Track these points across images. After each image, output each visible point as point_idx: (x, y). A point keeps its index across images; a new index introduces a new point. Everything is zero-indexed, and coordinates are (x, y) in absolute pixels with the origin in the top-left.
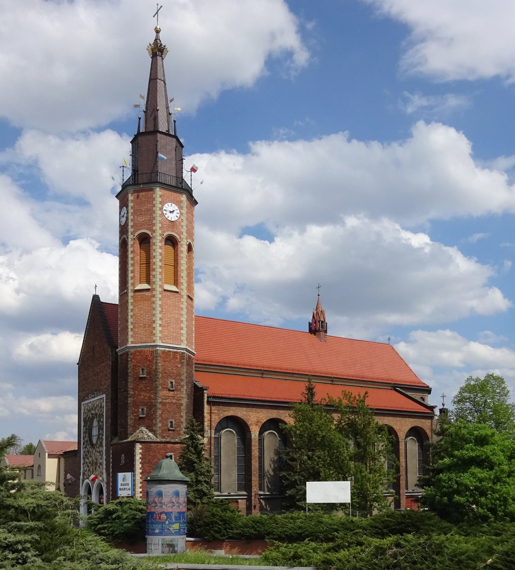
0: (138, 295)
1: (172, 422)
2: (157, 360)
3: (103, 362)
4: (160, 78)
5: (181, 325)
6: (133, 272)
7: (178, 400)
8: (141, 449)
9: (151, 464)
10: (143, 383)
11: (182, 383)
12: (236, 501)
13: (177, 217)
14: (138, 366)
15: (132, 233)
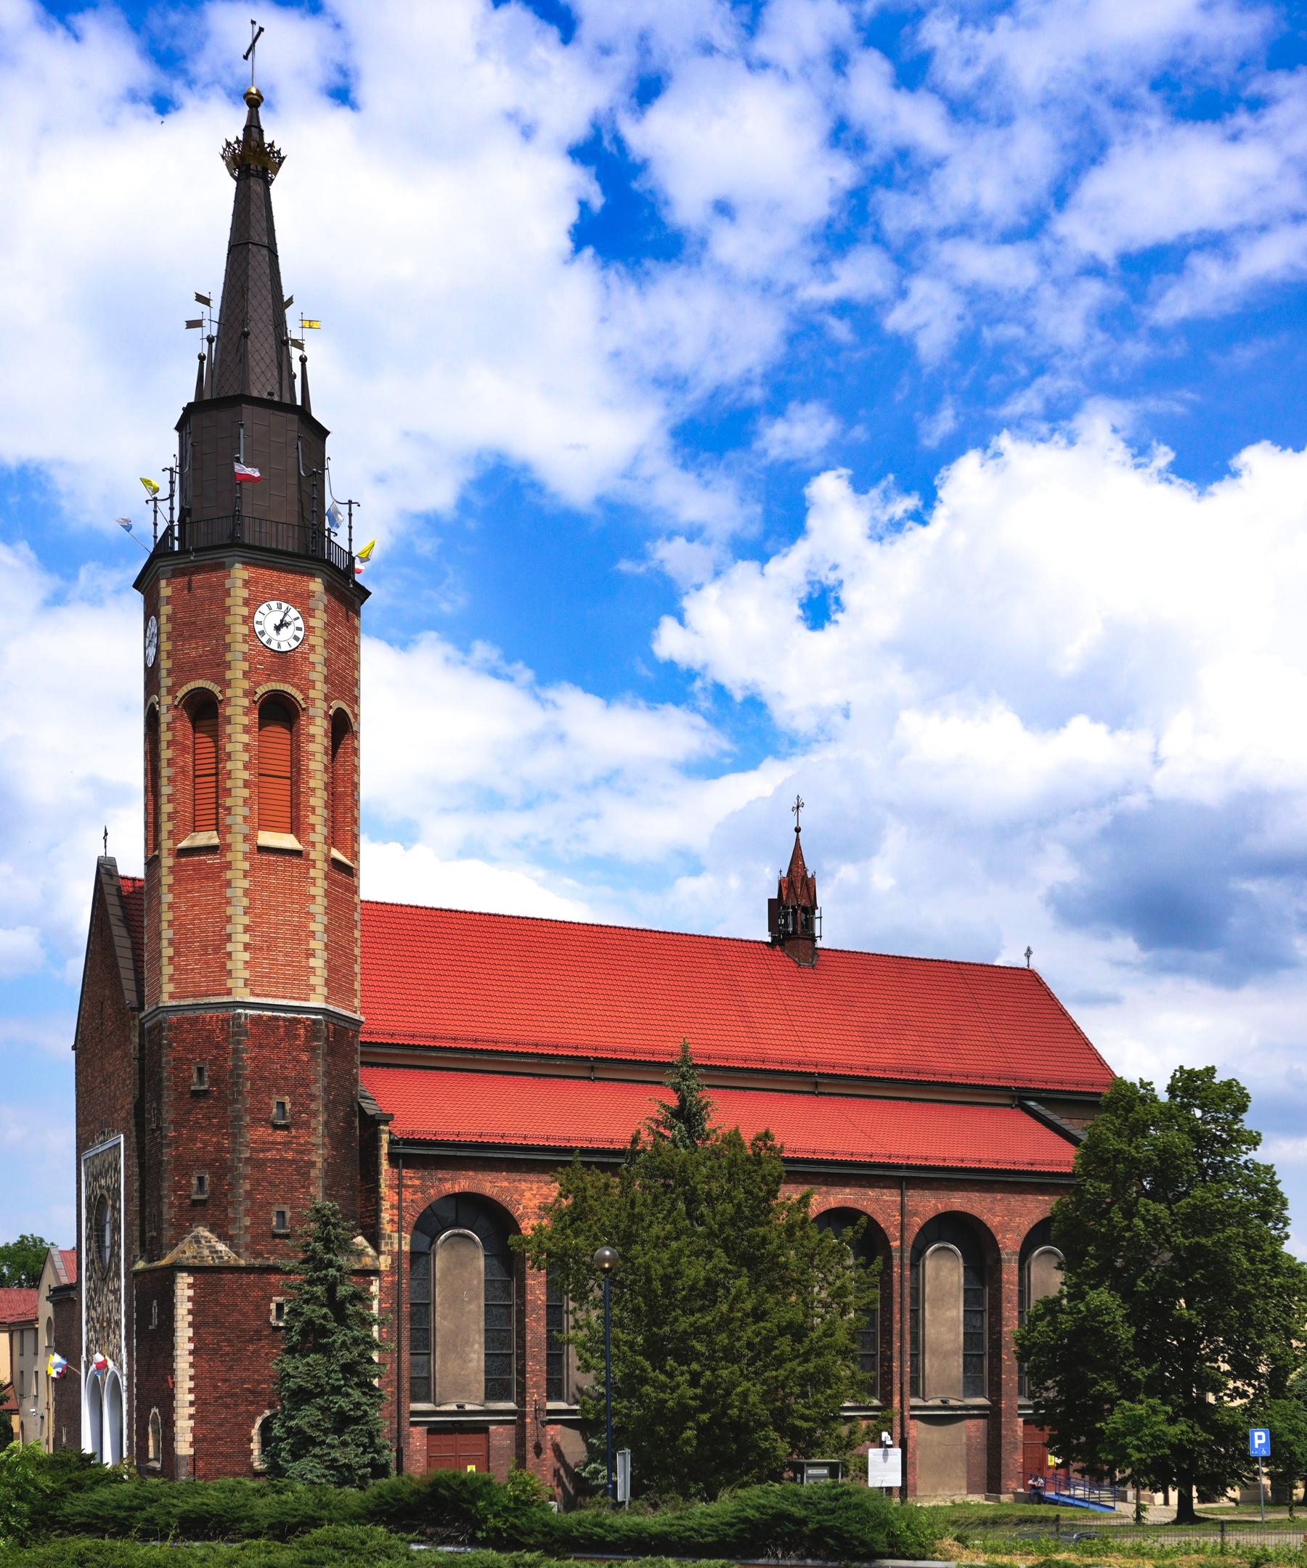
2: (239, 1042)
4: (256, 239)
7: (302, 1152)
8: (190, 1286)
10: (201, 1108)
11: (313, 1106)
12: (482, 1429)
13: (296, 638)
15: (171, 691)
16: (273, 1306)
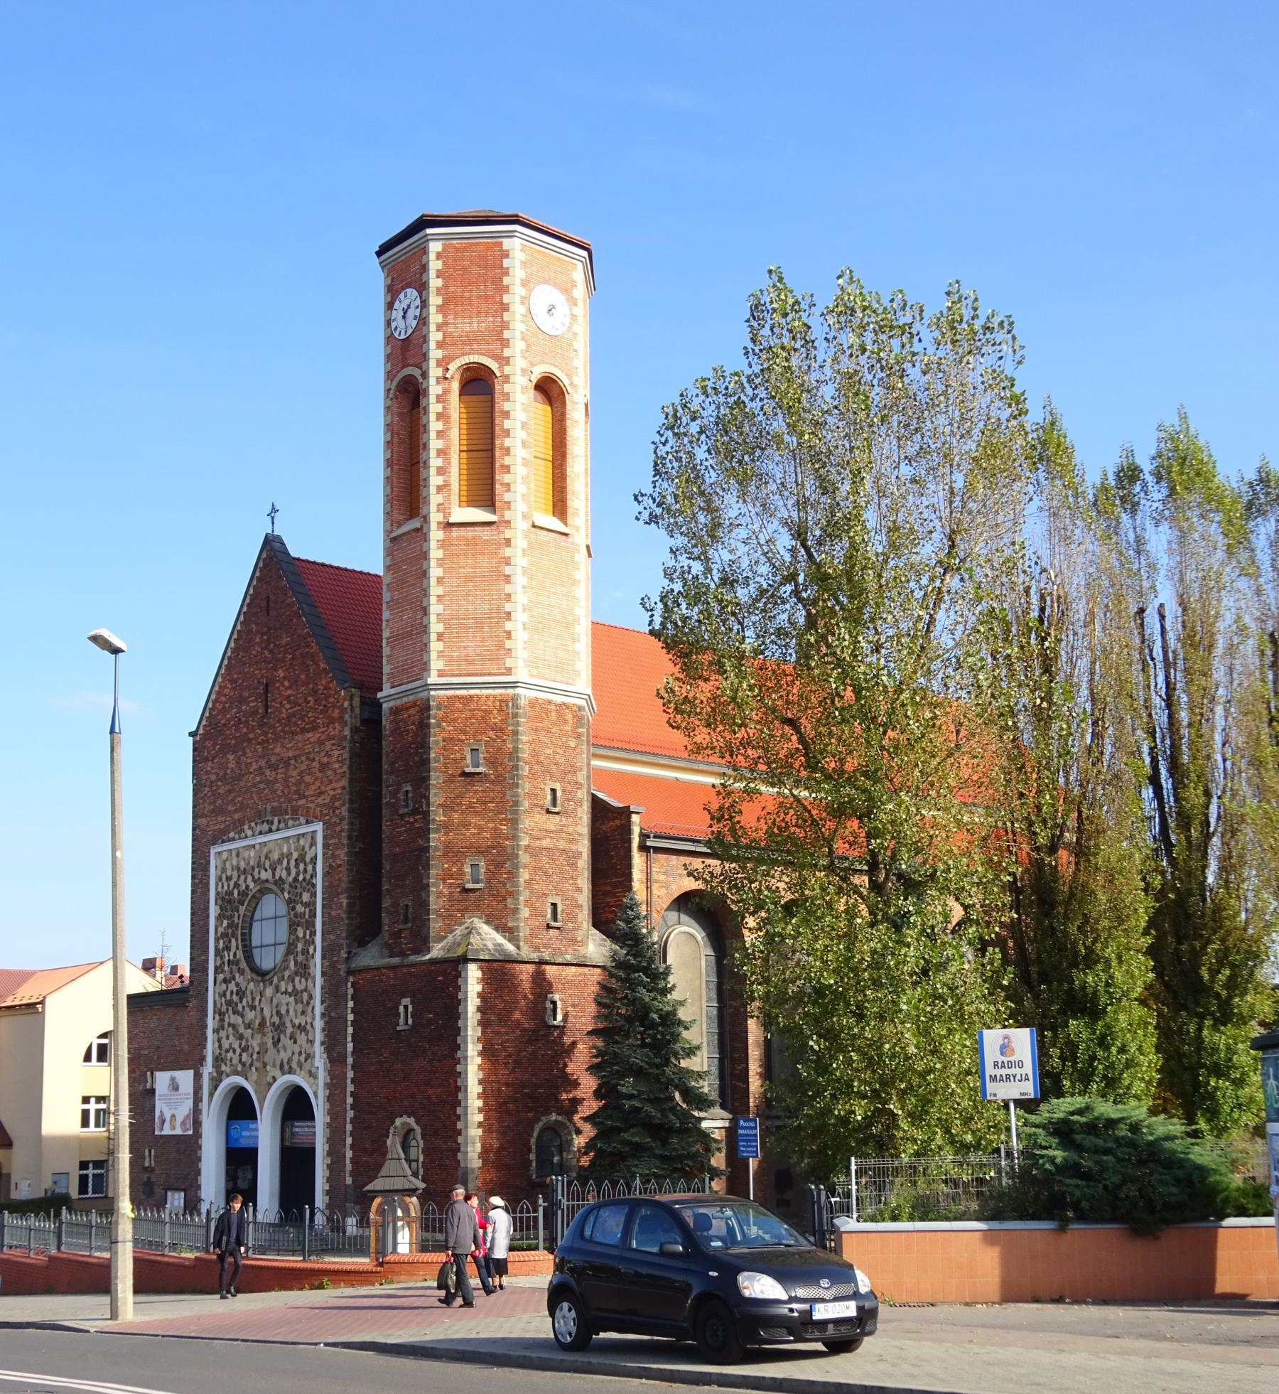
1: (554, 905)
3: (314, 728)
6: (441, 471)
7: (570, 842)
10: (476, 792)
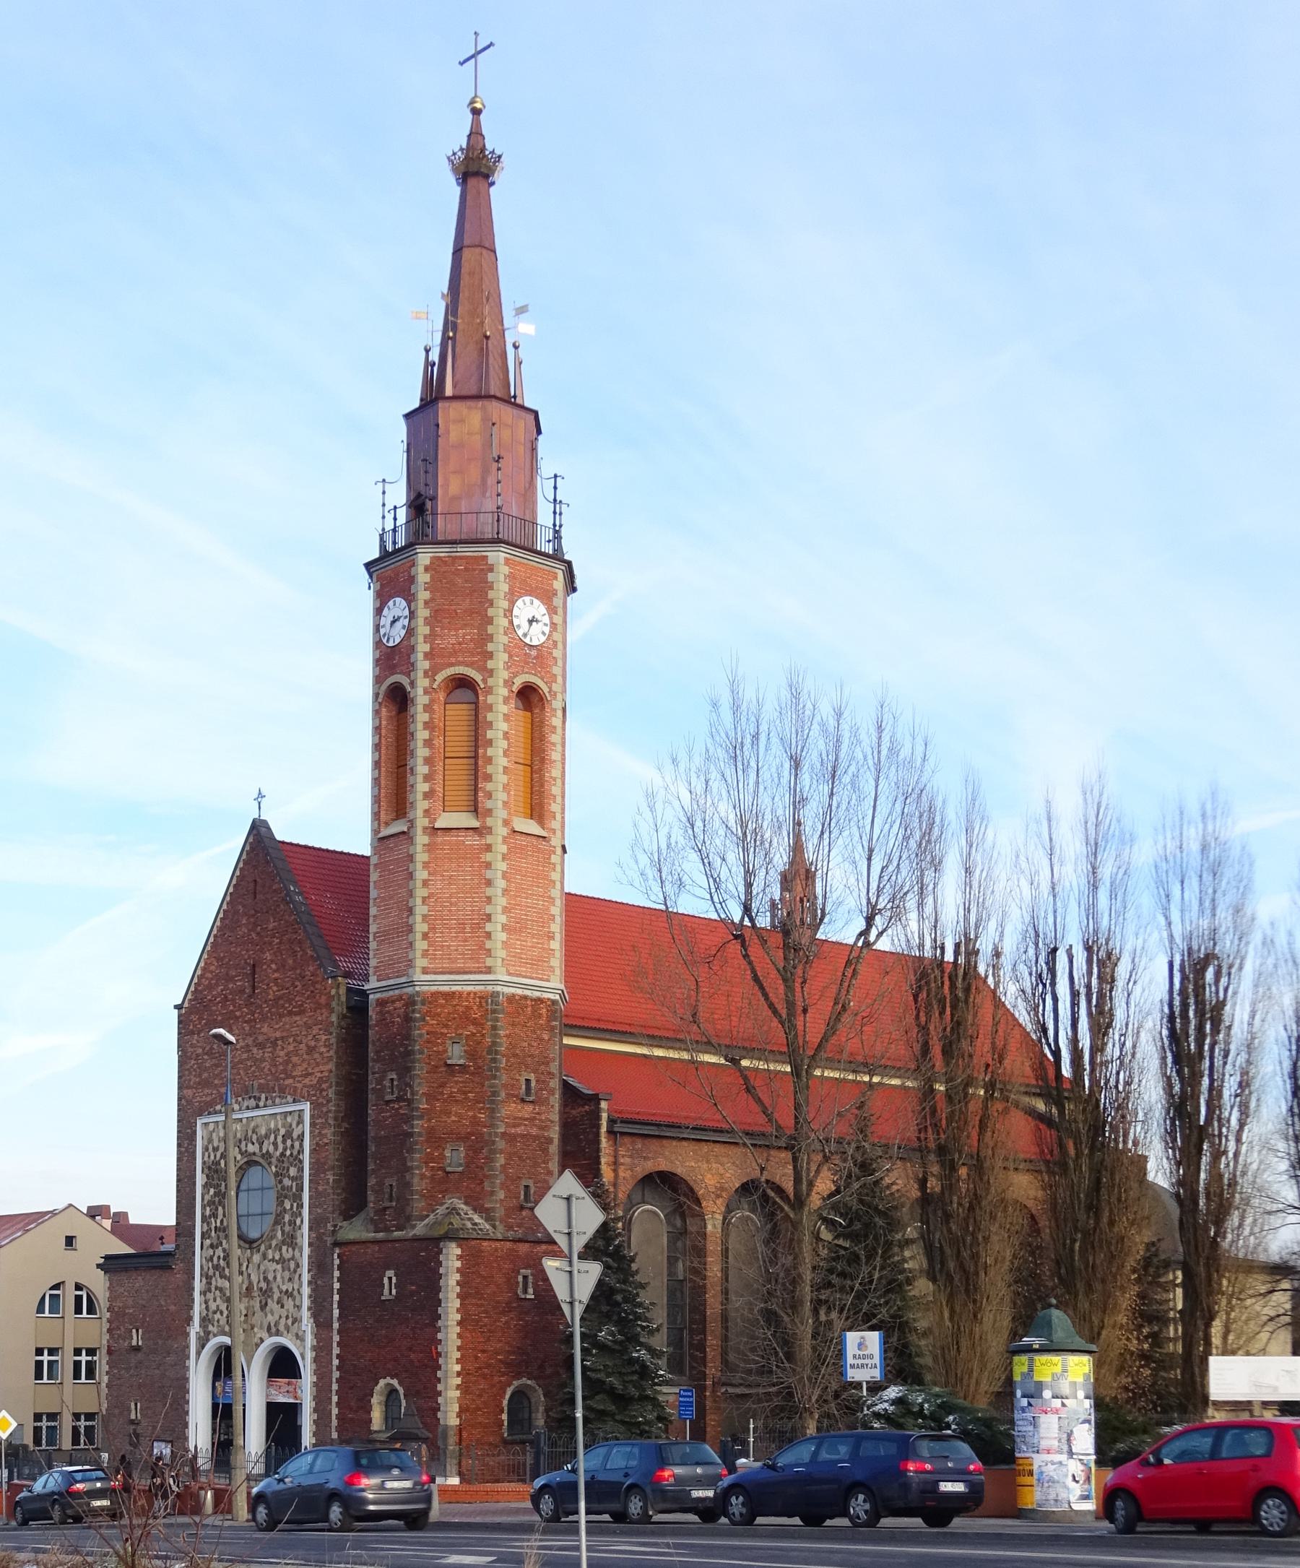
0: (442, 844)
2: (497, 1020)
3: (301, 1013)
5: (549, 927)
8: (460, 1257)
9: (480, 1299)
10: (457, 1082)
13: (543, 633)
14: (442, 1033)
16: (520, 1279)
